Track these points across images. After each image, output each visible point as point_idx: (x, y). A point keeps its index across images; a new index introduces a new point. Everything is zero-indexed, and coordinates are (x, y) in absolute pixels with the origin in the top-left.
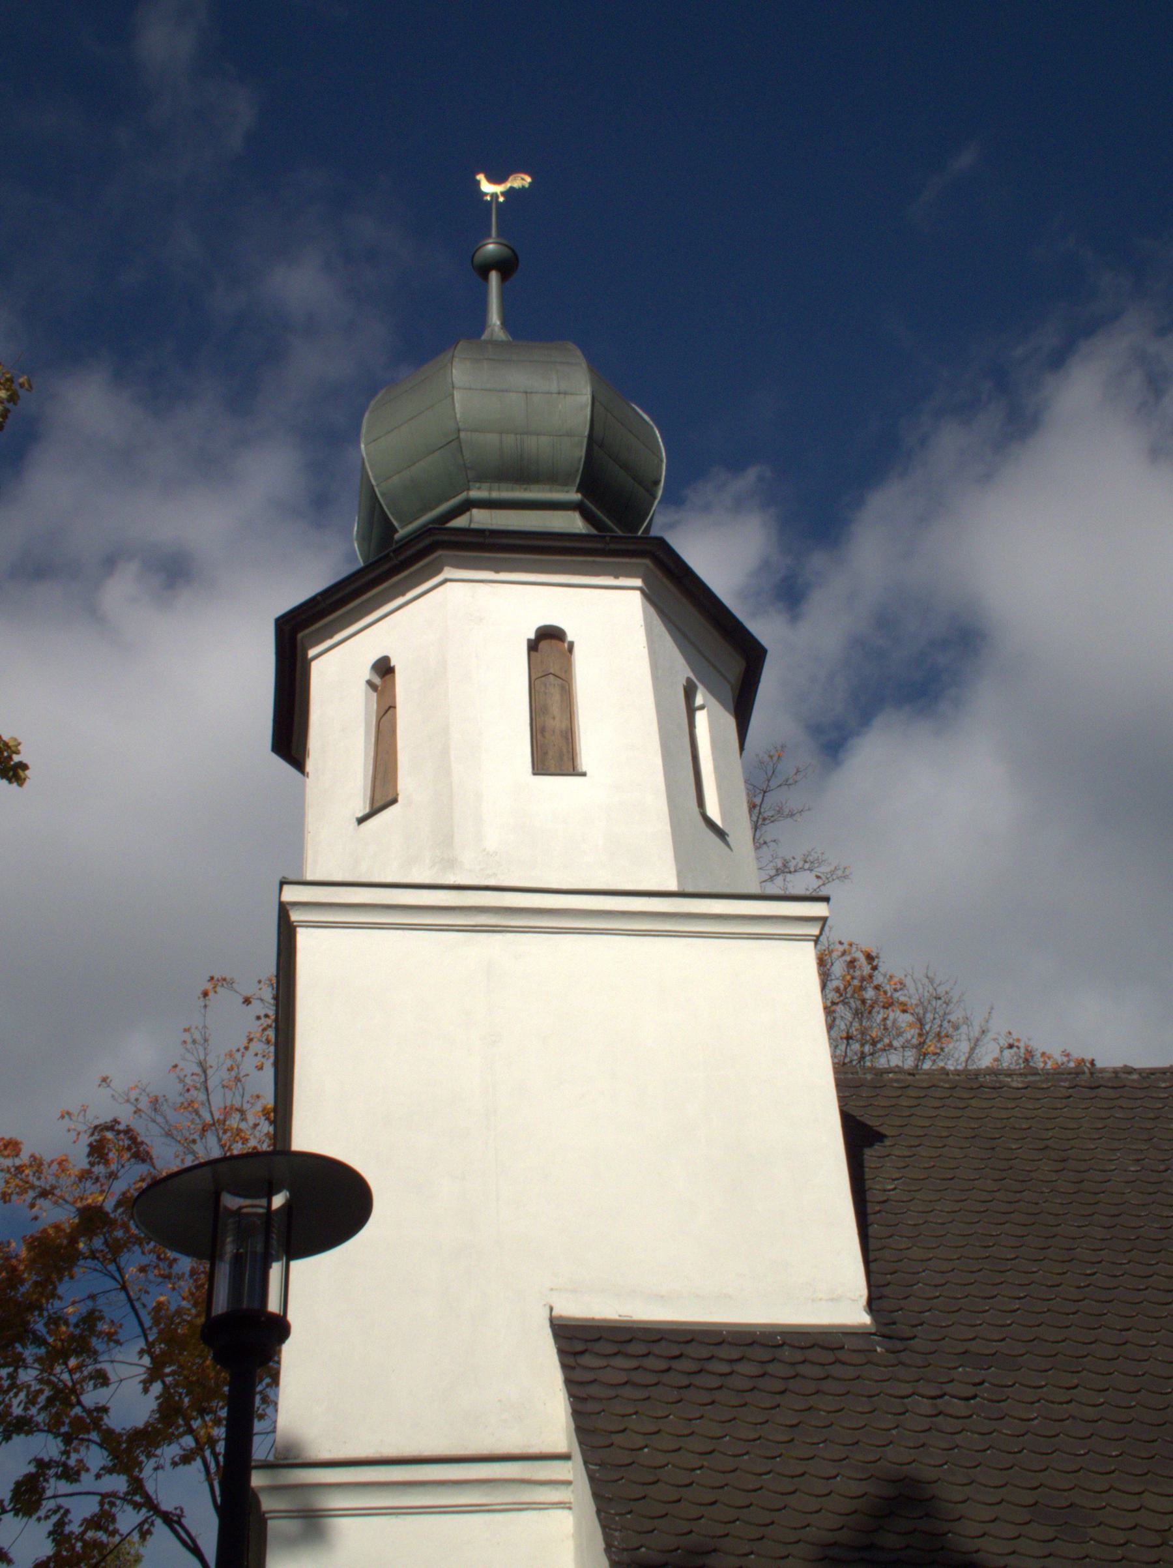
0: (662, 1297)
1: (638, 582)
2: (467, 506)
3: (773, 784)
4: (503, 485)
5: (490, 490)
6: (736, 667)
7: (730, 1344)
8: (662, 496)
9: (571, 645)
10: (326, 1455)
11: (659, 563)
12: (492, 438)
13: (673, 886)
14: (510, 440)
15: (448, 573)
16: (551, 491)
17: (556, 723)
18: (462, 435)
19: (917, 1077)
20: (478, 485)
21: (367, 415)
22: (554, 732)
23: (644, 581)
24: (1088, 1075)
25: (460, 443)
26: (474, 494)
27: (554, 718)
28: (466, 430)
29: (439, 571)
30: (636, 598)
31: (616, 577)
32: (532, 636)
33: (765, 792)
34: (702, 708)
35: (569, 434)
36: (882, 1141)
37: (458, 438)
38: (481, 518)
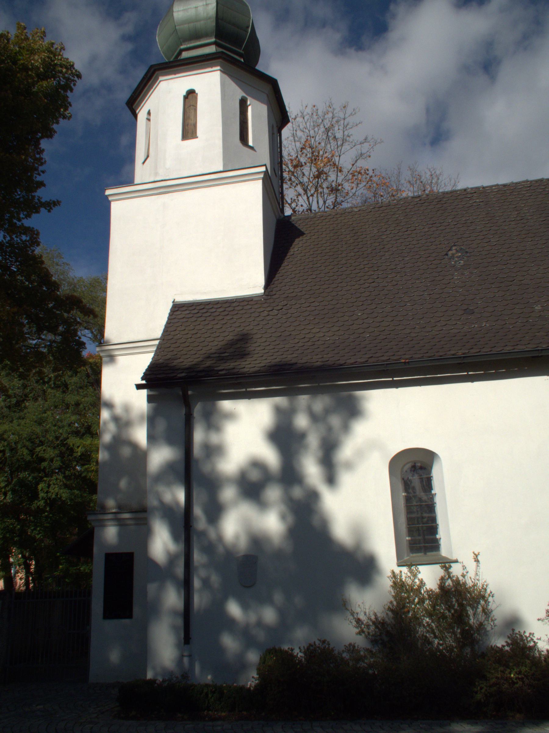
0: (205, 293)
1: (219, 68)
2: (182, 51)
3: (347, 116)
4: (192, 41)
5: (187, 45)
6: (268, 88)
7: (220, 303)
8: (251, 32)
9: (197, 94)
10: (116, 342)
11: (224, 59)
12: (186, 26)
13: (221, 169)
14: (191, 25)
15: (161, 78)
16: (207, 39)
17: (191, 122)
18: (177, 27)
19: (327, 213)
20: (184, 43)
21: (159, 26)
22: (191, 125)
23: (221, 67)
24: (380, 203)
25: (177, 32)
26: (182, 47)
27: (191, 120)
28: (178, 26)
29: (158, 79)
30: (218, 73)
31: (212, 67)
32: (185, 94)
33: (344, 119)
34: (250, 105)
35: (210, 18)
36: (303, 235)
37: (176, 29)
38: (185, 55)
